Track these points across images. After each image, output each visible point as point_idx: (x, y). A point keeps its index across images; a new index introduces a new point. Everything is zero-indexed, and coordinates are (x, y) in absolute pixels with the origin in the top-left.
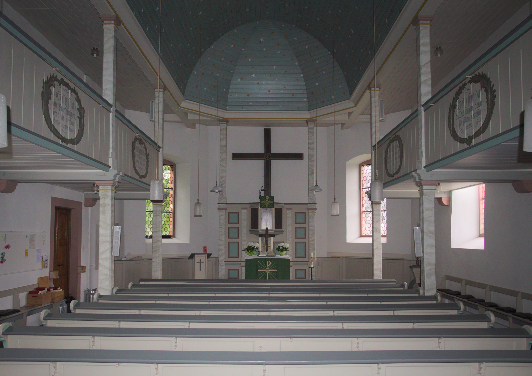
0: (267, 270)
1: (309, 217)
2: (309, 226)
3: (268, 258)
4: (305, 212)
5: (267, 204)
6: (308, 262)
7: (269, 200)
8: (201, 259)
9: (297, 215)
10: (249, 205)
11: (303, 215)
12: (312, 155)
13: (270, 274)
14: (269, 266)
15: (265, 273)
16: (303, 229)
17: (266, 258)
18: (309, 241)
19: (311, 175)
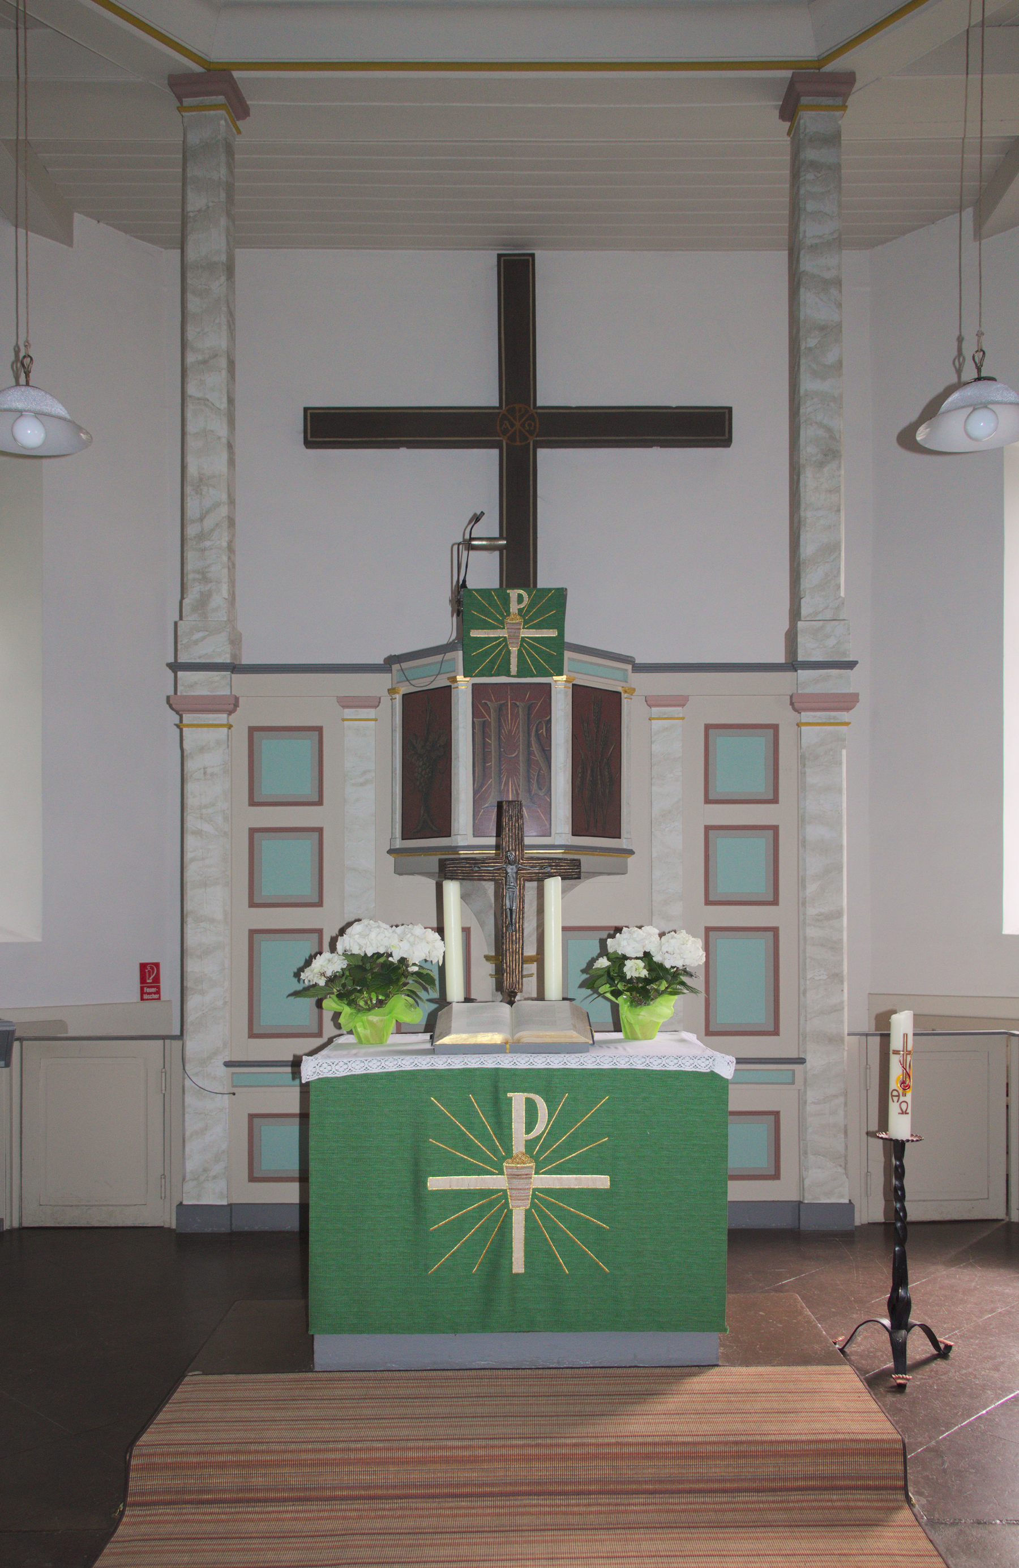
0: (512, 1176)
2: (802, 821)
3: (522, 1062)
4: (775, 728)
5: (514, 650)
7: (528, 618)
9: (722, 742)
10: (384, 680)
11: (759, 743)
12: (822, 328)
13: (543, 1216)
15: (491, 1205)
16: (761, 843)
17: (506, 1062)
19: (821, 465)
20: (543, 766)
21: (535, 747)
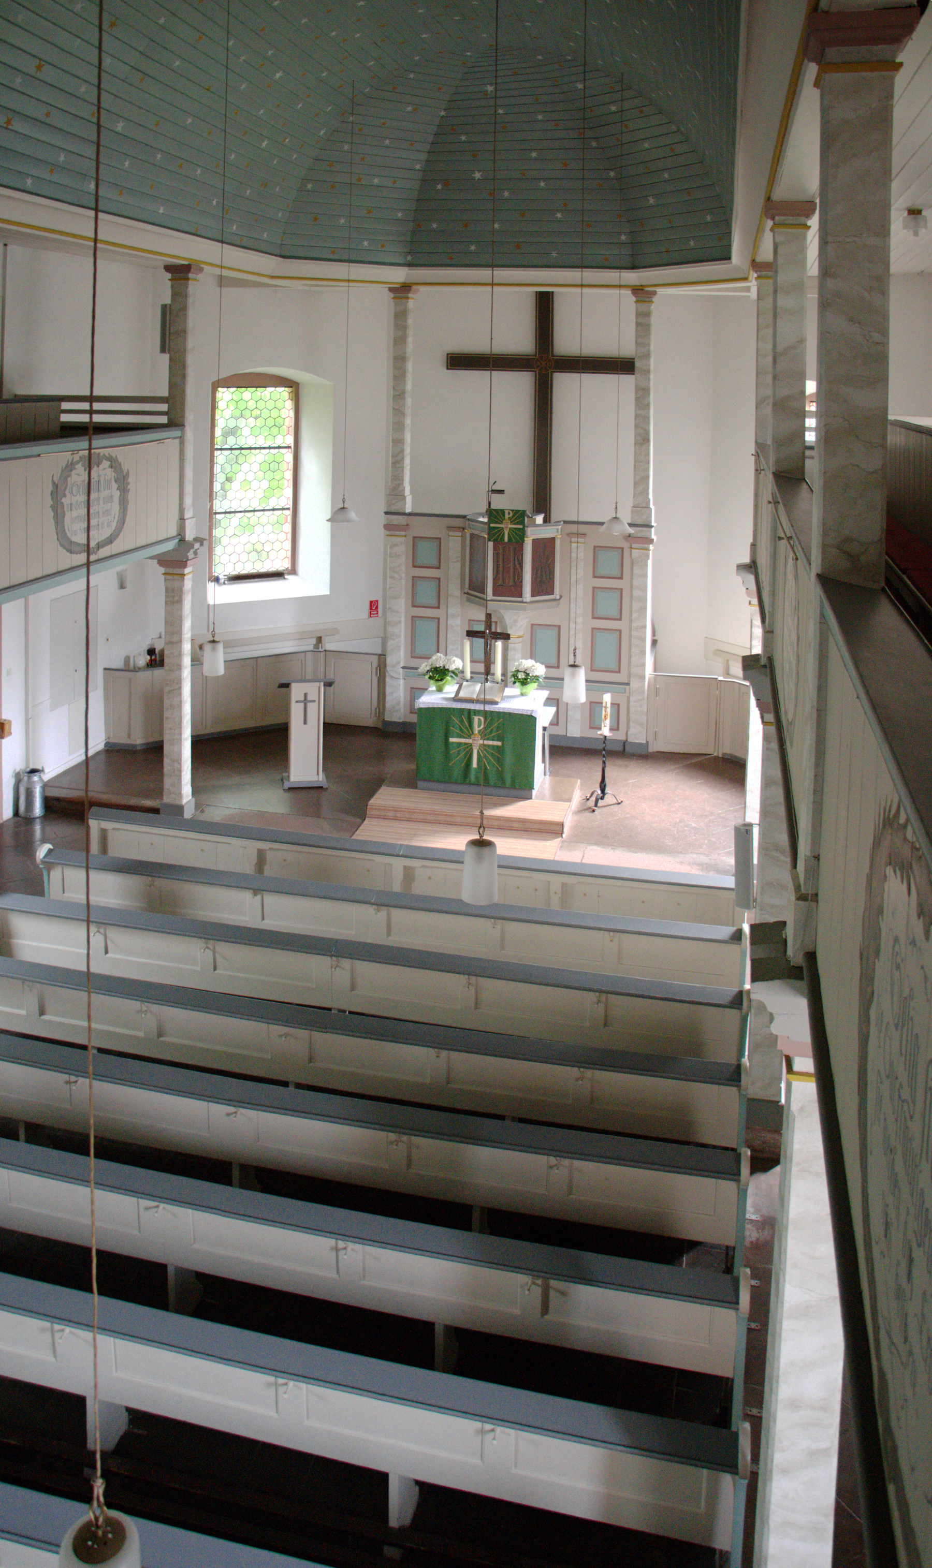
1: (632, 562)
6: (627, 687)
8: (306, 695)
14: (479, 731)
16: (616, 595)
18: (630, 630)
20: (520, 570)
21: (517, 564)
